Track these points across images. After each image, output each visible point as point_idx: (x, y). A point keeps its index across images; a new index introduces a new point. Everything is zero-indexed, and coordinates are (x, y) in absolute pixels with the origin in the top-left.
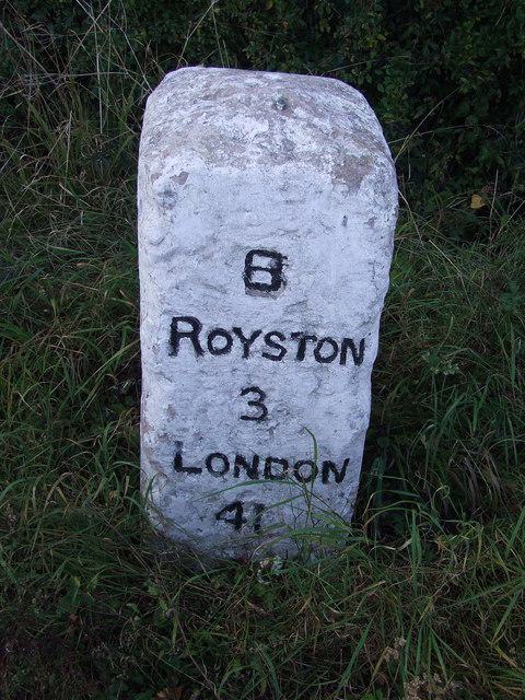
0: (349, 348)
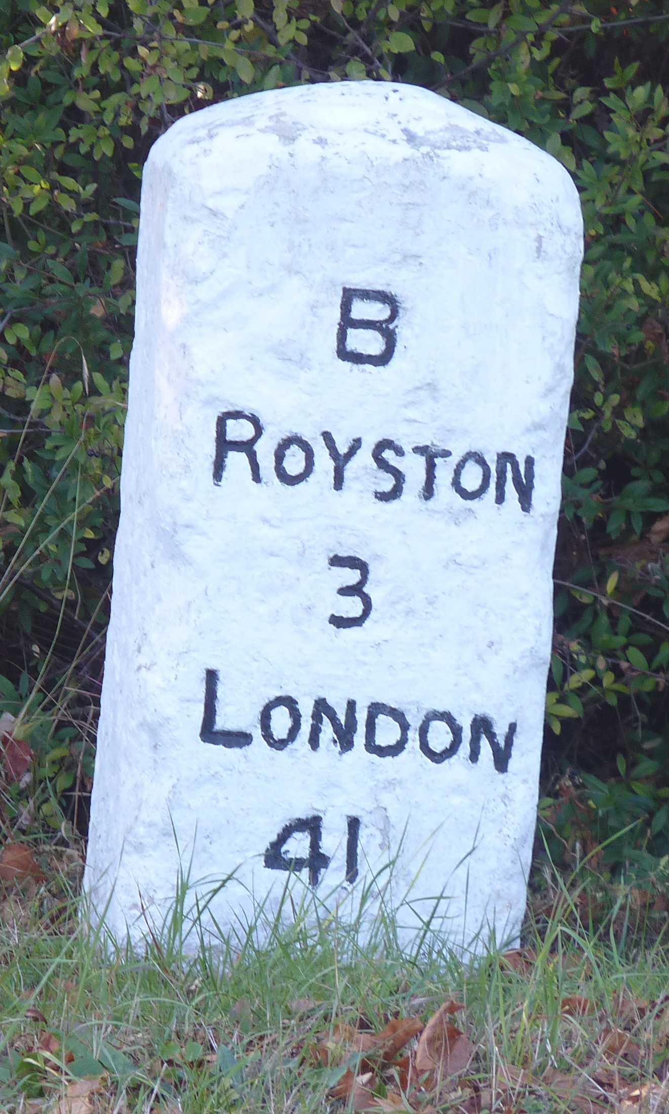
0: (511, 476)
